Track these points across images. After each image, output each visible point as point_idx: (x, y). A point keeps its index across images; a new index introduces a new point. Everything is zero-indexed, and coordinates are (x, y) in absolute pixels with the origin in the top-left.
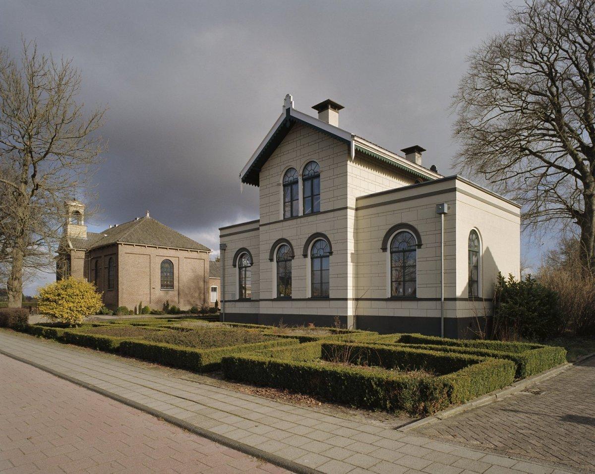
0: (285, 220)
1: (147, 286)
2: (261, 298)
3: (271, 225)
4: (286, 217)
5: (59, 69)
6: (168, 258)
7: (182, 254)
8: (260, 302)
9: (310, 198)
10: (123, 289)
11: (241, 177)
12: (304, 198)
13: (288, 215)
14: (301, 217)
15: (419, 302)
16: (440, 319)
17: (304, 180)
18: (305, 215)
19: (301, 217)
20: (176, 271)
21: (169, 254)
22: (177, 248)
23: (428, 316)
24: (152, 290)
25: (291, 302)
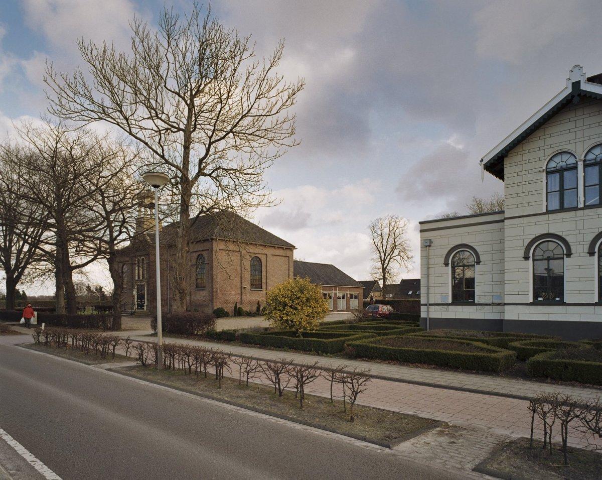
0: (548, 212)
1: (239, 286)
2: (506, 302)
3: (525, 219)
4: (549, 209)
5: (100, 46)
6: (257, 255)
7: (269, 251)
8: (505, 306)
9: (598, 186)
10: (217, 288)
11: (484, 162)
12: (585, 187)
13: (555, 205)
14: (580, 209)
15: (568, 307)
16: (427, 318)
17: (585, 166)
18: (586, 207)
19: (580, 209)
20: (264, 270)
21: (259, 250)
22: (265, 244)
23: (486, 318)
24: (243, 290)
25: (565, 307)
